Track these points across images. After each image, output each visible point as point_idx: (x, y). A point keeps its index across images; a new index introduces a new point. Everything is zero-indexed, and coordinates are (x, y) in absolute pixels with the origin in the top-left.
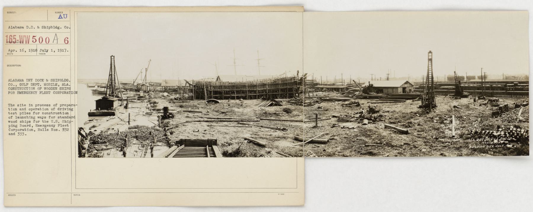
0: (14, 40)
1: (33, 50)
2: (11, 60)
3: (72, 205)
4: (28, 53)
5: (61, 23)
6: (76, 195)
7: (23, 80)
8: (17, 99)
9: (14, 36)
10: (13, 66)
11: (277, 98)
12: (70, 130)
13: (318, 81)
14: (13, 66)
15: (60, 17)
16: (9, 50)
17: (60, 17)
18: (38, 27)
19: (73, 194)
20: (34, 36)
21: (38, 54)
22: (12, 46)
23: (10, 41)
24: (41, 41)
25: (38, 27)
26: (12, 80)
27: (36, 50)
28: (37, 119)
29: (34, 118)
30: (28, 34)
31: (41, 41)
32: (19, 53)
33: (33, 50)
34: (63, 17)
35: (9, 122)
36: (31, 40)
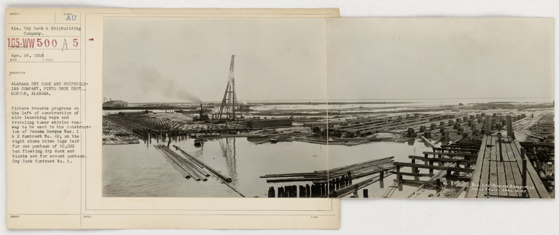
0: (17, 44)
1: (38, 56)
2: (14, 67)
3: (81, 228)
4: (33, 59)
5: (71, 23)
6: (86, 217)
7: (28, 84)
8: (22, 101)
9: (17, 39)
10: (17, 73)
11: (532, 161)
12: (80, 141)
13: (465, 103)
14: (17, 73)
15: (68, 18)
16: (12, 56)
17: (68, 18)
18: (47, 28)
19: (82, 216)
20: (74, 40)
21: (44, 60)
22: (16, 51)
23: (12, 44)
24: (47, 41)
25: (47, 28)
26: (16, 83)
27: (43, 55)
28: (44, 153)
29: (41, 152)
30: (33, 38)
31: (47, 41)
32: (23, 59)
33: (38, 56)
34: (71, 18)
35: (13, 127)
36: (36, 43)
